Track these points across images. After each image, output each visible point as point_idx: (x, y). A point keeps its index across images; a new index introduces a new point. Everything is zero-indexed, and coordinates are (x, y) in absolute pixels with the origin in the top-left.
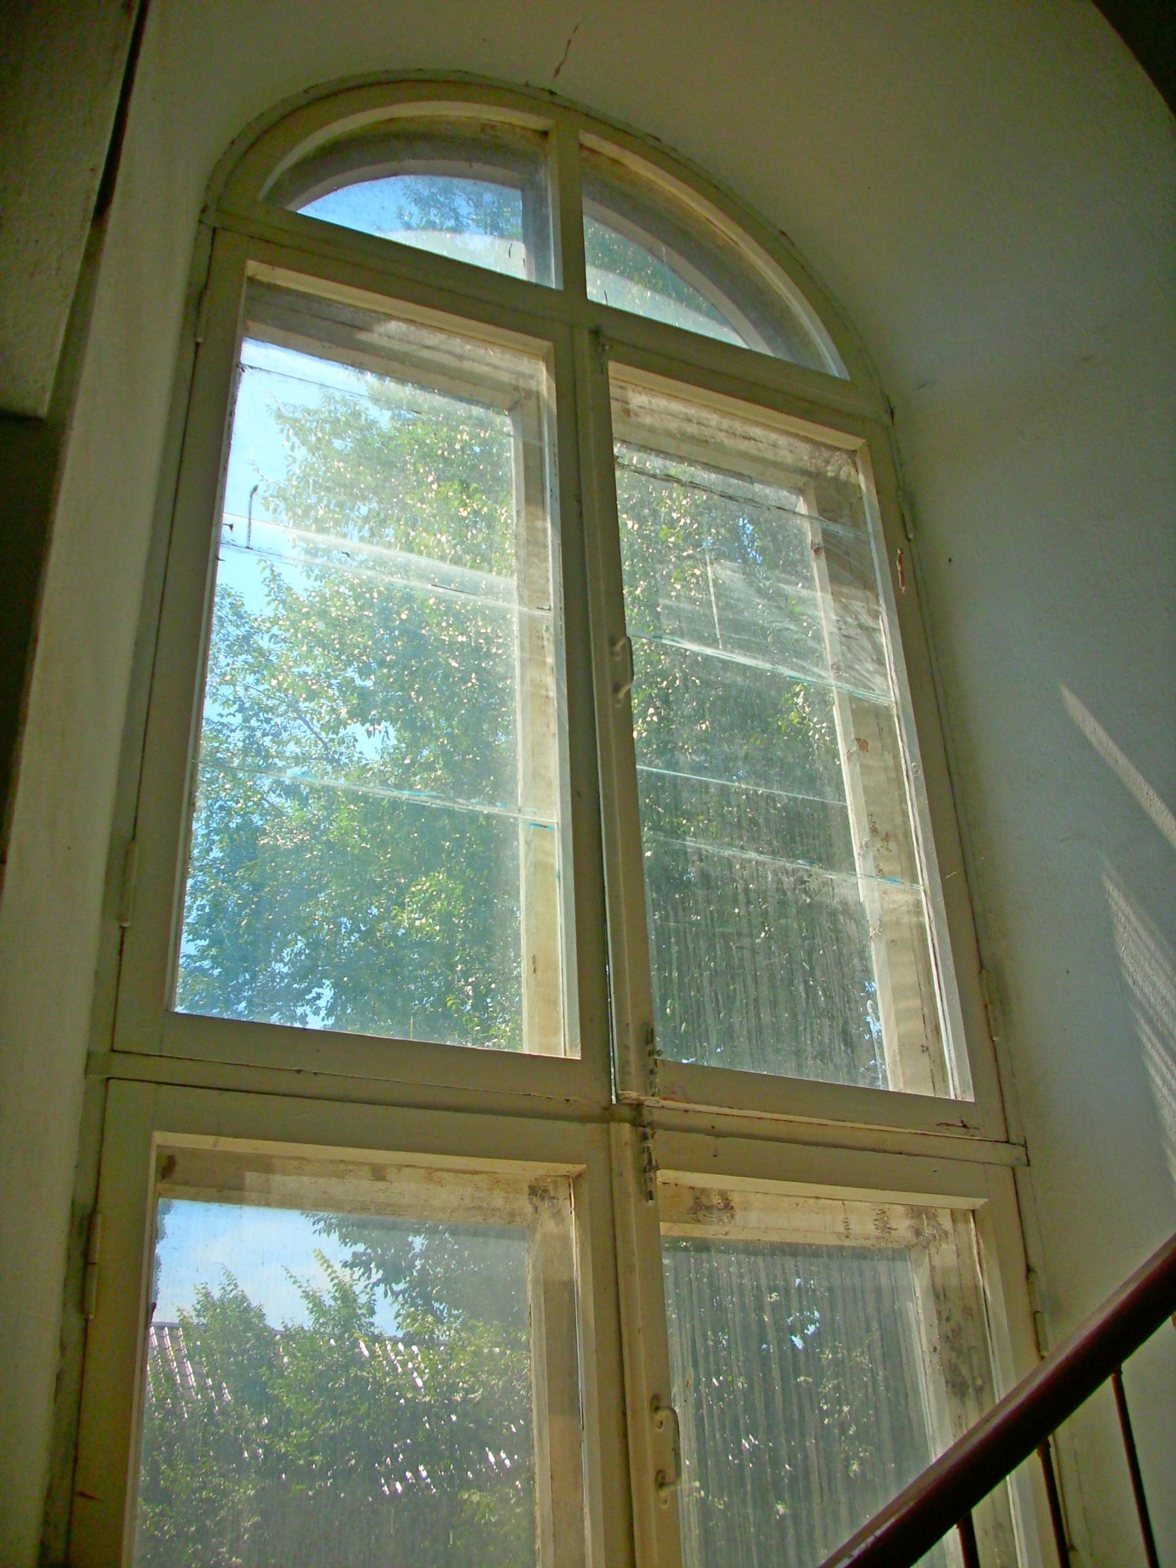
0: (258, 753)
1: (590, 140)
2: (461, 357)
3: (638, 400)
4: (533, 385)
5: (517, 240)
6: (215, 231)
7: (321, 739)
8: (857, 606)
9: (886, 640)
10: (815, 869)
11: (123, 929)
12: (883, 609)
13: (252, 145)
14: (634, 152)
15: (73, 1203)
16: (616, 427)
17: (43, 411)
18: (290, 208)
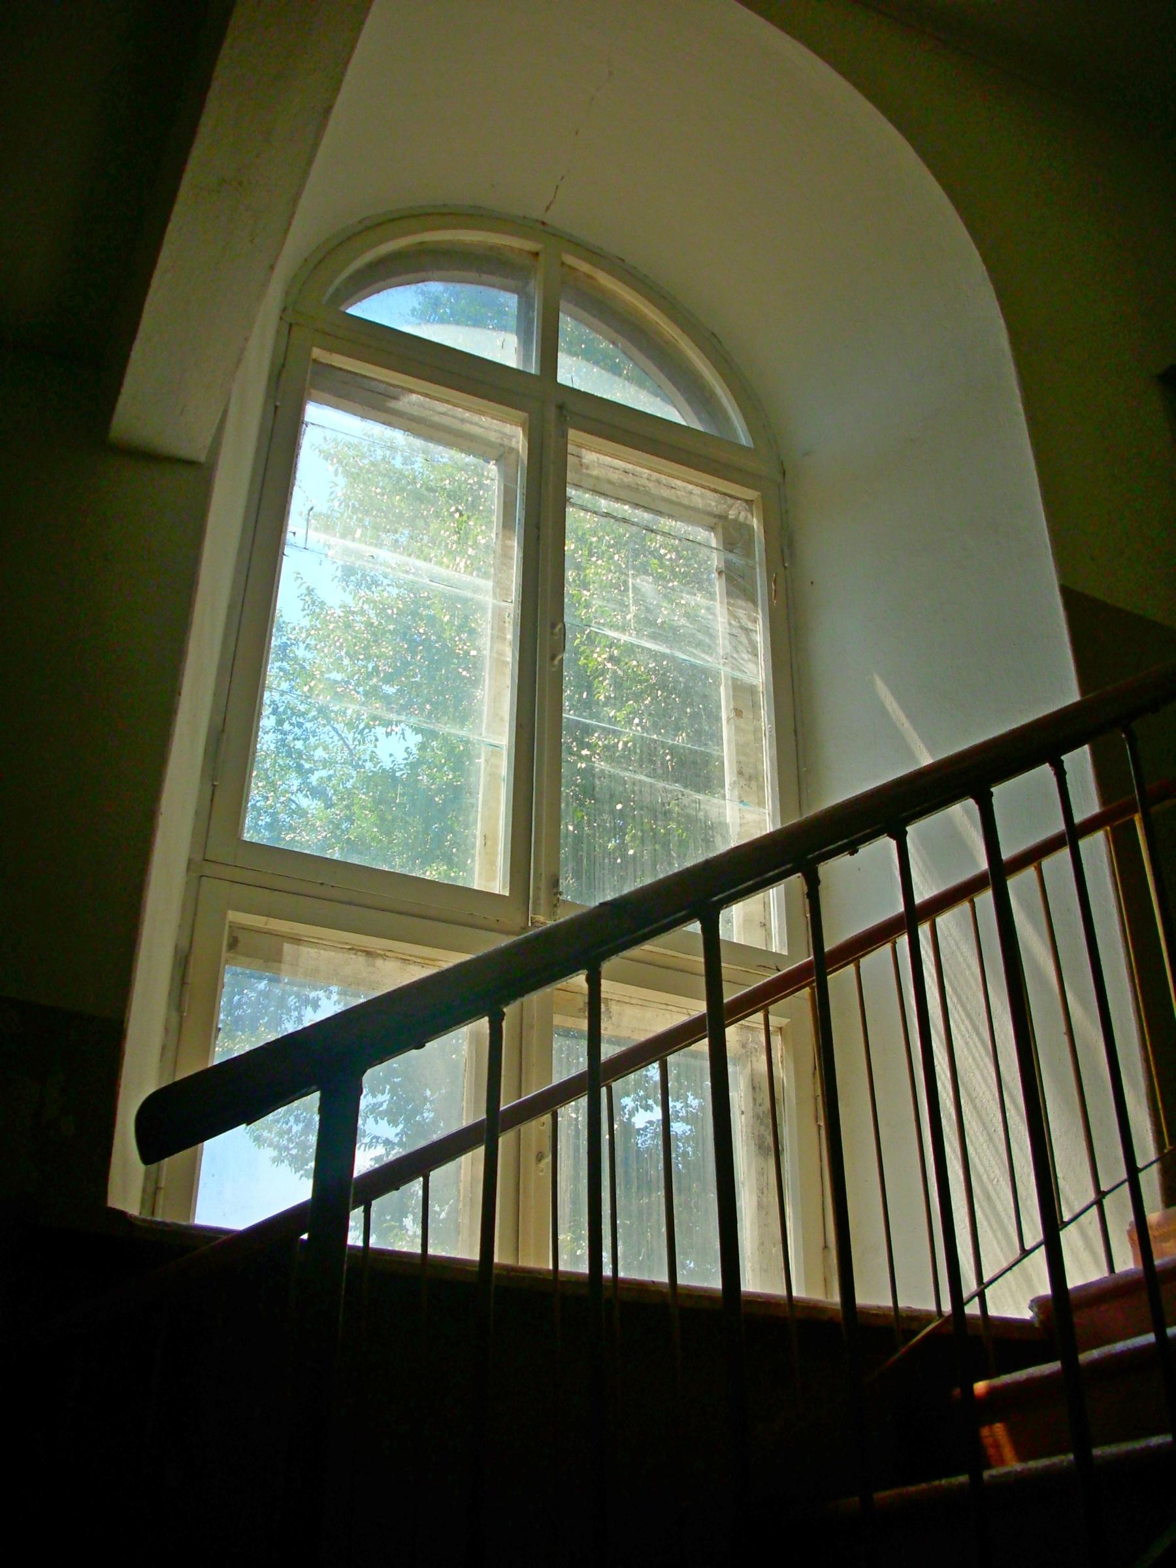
0: (289, 755)
1: (570, 260)
2: (463, 420)
3: (590, 457)
4: (513, 444)
5: (512, 332)
6: (291, 325)
7: (348, 746)
8: (741, 613)
9: (760, 638)
10: (687, 791)
11: (214, 786)
12: (760, 617)
13: (320, 262)
14: (603, 270)
15: (176, 947)
16: (570, 476)
17: (203, 459)
18: (342, 308)
